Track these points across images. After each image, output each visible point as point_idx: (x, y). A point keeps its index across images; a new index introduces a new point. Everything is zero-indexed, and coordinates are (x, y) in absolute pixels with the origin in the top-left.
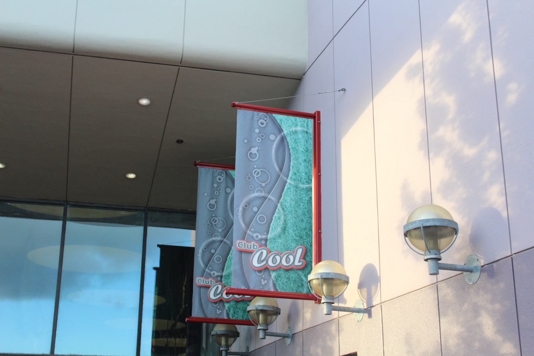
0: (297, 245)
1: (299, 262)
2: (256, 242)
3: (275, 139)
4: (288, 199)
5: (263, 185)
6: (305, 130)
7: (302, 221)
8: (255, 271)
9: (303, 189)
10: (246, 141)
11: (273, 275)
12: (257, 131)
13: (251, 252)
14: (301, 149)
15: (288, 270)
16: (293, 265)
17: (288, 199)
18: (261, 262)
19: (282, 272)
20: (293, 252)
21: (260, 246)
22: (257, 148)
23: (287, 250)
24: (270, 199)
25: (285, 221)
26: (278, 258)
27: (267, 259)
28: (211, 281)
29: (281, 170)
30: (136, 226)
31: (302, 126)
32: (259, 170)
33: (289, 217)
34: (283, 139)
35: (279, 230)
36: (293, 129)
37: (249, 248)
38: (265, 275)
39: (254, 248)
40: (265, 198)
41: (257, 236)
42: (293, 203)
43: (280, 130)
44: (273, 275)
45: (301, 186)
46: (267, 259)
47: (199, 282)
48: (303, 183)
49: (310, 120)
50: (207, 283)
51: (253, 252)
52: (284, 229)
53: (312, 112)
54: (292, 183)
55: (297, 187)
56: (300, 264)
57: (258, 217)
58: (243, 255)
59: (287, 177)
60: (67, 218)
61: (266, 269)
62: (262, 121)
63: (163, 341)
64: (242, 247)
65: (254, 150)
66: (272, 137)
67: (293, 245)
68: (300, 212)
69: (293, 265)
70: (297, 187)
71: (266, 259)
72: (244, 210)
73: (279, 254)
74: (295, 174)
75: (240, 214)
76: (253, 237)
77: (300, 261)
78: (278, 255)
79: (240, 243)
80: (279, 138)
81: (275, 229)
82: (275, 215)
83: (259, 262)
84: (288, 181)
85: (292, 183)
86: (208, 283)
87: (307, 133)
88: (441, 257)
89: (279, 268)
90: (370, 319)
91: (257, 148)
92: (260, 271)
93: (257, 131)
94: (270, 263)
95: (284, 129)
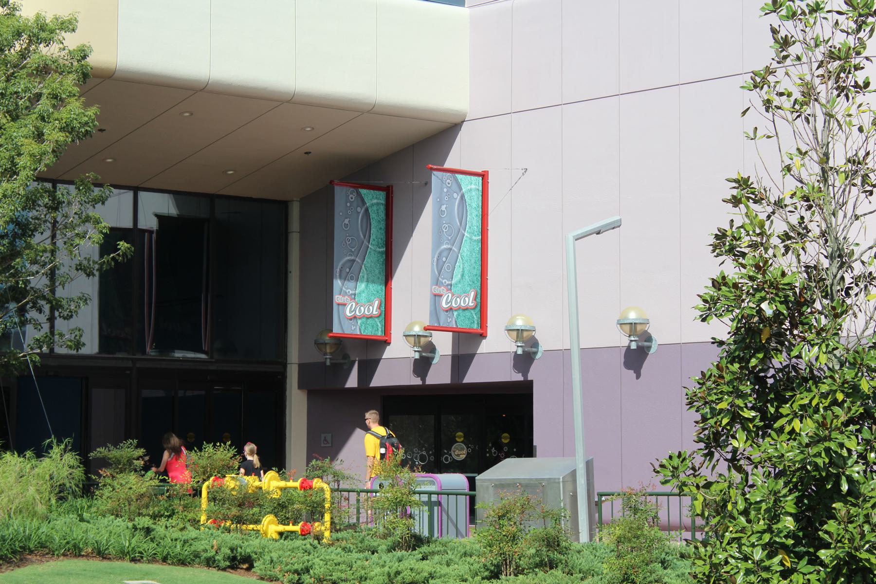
0: (375, 298)
2: (444, 287)
3: (361, 211)
4: (465, 249)
5: (450, 238)
6: (477, 187)
7: (474, 268)
8: (444, 310)
9: (475, 241)
10: (438, 200)
11: (455, 313)
12: (445, 190)
13: (345, 305)
14: (474, 205)
15: (368, 318)
17: (465, 249)
19: (460, 311)
20: (468, 295)
21: (447, 291)
22: (445, 206)
23: (464, 293)
24: (357, 262)
25: (463, 269)
26: (362, 308)
27: (355, 310)
29: (461, 224)
31: (475, 184)
32: (447, 226)
33: (466, 265)
34: (463, 197)
35: (459, 276)
36: (469, 187)
38: (449, 314)
40: (450, 249)
41: (445, 282)
42: (469, 253)
43: (363, 202)
44: (455, 313)
45: (474, 238)
48: (475, 236)
49: (381, 192)
52: (463, 275)
53: (480, 170)
54: (468, 236)
55: (471, 239)
56: (377, 313)
57: (446, 266)
58: (340, 307)
59: (465, 230)
61: (355, 317)
62: (448, 181)
63: (534, 350)
65: (443, 208)
66: (455, 195)
67: (468, 288)
68: (473, 261)
70: (471, 239)
72: (341, 271)
73: (459, 297)
74: (470, 228)
75: (338, 275)
76: (442, 283)
80: (363, 209)
81: (457, 277)
82: (457, 264)
84: (466, 234)
85: (468, 236)
87: (478, 190)
89: (458, 308)
91: (445, 206)
92: (447, 311)
93: (445, 190)
94: (358, 313)
95: (463, 188)
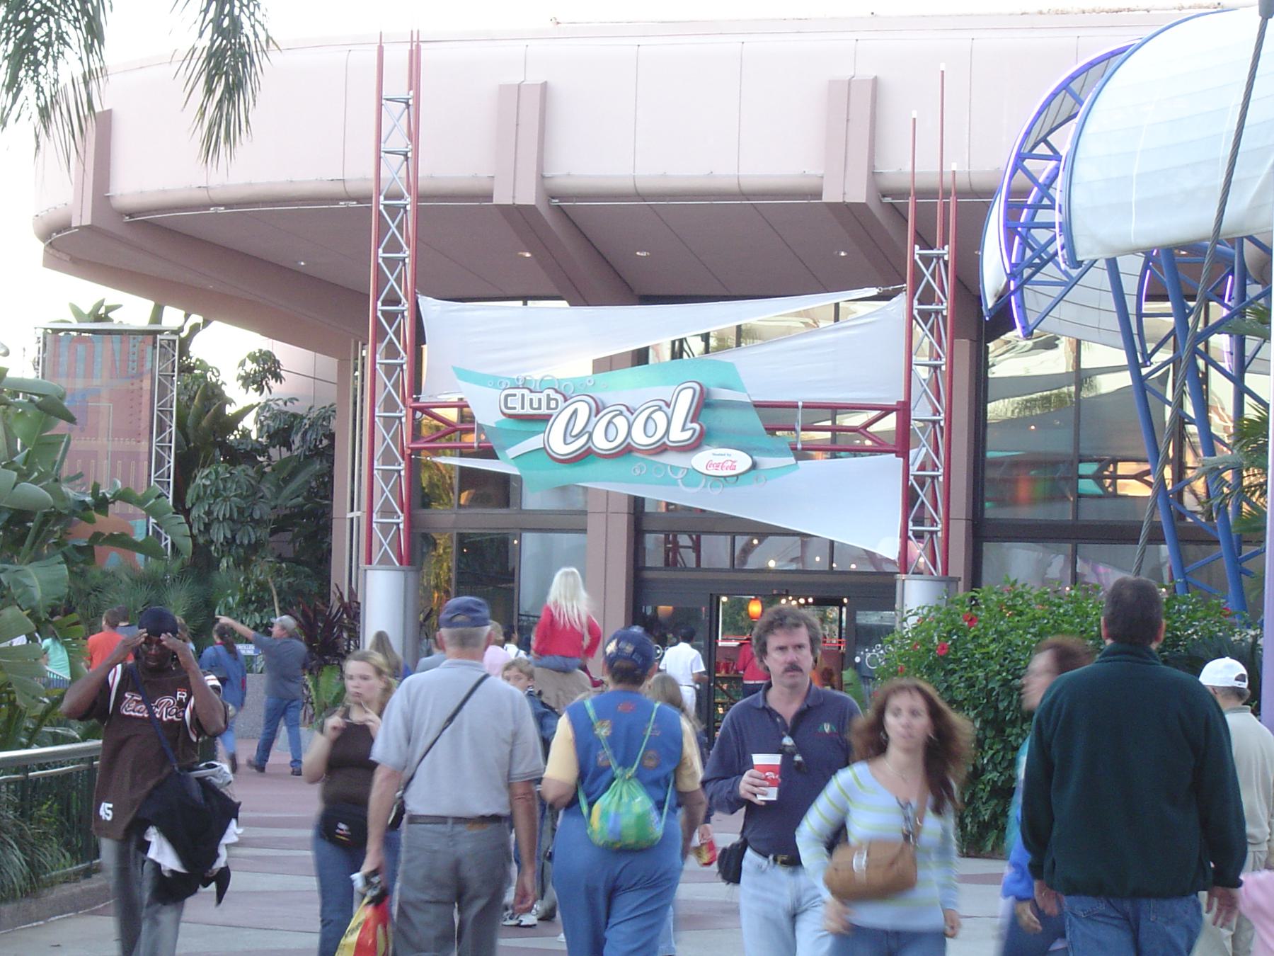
1: (683, 429)
16: (665, 440)
18: (573, 439)
28: (549, 399)
30: (137, 945)
37: (535, 409)
39: (549, 408)
46: (591, 430)
47: (509, 405)
50: (535, 405)
51: (548, 421)
56: (688, 434)
60: (56, 419)
64: (515, 408)
69: (665, 440)
71: (587, 430)
77: (686, 428)
78: (621, 413)
79: (509, 398)
83: (569, 439)
86: (539, 408)
88: (380, 680)
90: (232, 751)
